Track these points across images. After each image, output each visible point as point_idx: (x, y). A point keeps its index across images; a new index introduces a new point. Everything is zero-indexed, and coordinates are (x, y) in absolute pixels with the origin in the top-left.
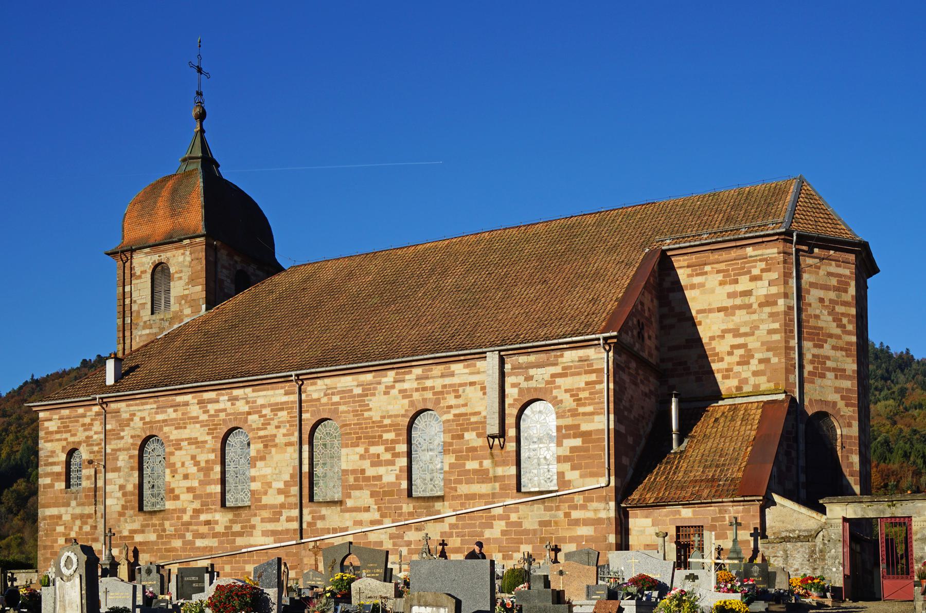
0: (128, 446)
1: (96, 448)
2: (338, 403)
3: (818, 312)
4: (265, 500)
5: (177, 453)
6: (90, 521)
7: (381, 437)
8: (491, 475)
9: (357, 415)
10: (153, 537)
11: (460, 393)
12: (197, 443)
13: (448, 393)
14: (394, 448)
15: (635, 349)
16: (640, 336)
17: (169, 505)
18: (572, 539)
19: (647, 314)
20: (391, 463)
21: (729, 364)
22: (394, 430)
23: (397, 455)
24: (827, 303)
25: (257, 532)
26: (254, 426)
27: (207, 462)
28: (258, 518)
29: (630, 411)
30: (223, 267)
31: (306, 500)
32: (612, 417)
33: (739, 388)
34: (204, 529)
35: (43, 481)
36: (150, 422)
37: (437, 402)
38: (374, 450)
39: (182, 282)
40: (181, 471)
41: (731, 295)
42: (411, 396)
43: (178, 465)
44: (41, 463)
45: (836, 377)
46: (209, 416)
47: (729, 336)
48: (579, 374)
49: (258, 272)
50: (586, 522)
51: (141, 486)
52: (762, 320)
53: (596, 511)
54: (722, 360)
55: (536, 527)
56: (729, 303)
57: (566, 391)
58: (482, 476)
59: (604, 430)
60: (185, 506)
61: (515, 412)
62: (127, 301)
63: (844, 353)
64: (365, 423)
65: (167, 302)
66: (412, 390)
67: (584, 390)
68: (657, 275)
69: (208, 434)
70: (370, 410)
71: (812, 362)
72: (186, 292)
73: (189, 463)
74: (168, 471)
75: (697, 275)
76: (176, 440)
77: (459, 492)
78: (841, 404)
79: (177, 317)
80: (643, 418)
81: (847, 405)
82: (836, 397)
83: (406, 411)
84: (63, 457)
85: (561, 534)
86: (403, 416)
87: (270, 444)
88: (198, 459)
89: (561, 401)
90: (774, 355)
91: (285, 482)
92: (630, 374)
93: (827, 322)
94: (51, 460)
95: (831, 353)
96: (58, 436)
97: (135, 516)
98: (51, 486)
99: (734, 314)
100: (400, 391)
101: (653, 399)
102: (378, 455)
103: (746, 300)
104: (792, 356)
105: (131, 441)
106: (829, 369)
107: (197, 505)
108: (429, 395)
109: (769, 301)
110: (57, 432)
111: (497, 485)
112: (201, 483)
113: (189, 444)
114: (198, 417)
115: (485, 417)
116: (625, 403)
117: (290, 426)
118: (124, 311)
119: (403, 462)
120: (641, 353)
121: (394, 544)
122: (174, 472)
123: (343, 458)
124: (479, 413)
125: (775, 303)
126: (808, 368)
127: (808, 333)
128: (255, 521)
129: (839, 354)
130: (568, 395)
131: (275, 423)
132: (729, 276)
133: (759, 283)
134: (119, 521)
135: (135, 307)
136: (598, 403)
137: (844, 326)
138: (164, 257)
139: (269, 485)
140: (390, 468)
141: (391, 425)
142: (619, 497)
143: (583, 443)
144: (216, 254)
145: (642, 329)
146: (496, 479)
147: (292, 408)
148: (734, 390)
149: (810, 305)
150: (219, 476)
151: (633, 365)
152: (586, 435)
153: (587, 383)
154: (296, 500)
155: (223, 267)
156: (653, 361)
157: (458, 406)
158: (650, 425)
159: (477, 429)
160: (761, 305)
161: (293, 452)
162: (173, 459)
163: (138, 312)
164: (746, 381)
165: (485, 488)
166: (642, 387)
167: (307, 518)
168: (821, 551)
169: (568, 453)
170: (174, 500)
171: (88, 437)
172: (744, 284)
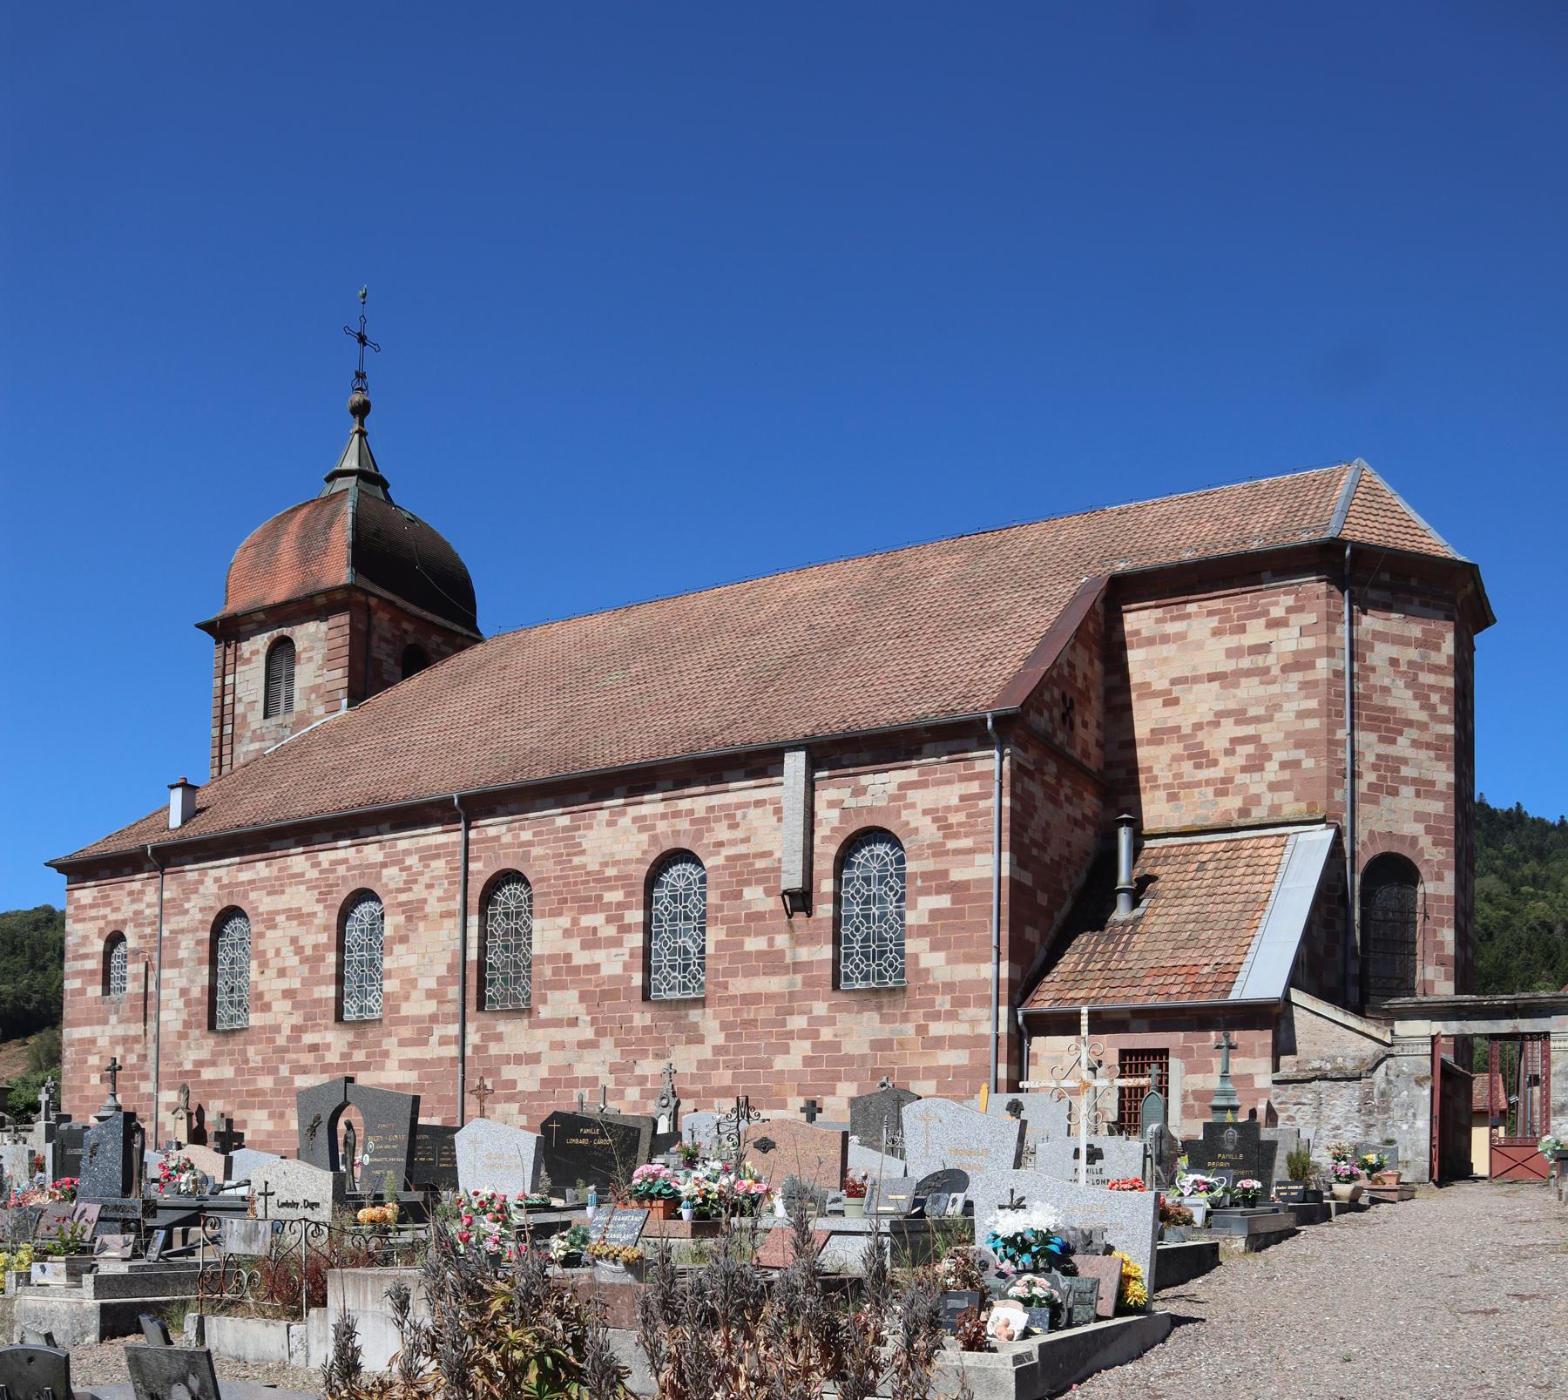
0: (196, 924)
1: (148, 930)
2: (530, 844)
3: (1387, 682)
4: (407, 1009)
5: (270, 934)
6: (138, 1048)
7: (600, 897)
8: (788, 960)
9: (560, 863)
10: (228, 1072)
11: (738, 819)
12: (302, 915)
13: (718, 819)
14: (621, 917)
15: (1057, 742)
16: (1067, 720)
17: (255, 1019)
18: (930, 1073)
19: (1080, 684)
20: (616, 942)
21: (1226, 770)
22: (623, 886)
23: (625, 929)
24: (1403, 668)
25: (391, 1063)
26: (392, 886)
27: (315, 947)
28: (394, 1040)
29: (1042, 847)
30: (382, 639)
31: (471, 1008)
32: (1006, 856)
33: (1244, 812)
34: (307, 1059)
35: (69, 985)
36: (230, 885)
37: (698, 836)
38: (587, 920)
39: (313, 666)
40: (275, 963)
41: (1231, 653)
42: (653, 827)
43: (271, 954)
44: (68, 955)
45: (1418, 794)
46: (321, 872)
47: (1227, 723)
48: (949, 782)
49: (444, 648)
50: (955, 1042)
51: (212, 990)
52: (1288, 696)
53: (973, 1022)
54: (1215, 763)
55: (866, 1050)
56: (1229, 666)
57: (925, 812)
58: (772, 962)
59: (990, 879)
60: (279, 1020)
61: (833, 849)
62: (228, 699)
63: (1432, 754)
64: (576, 876)
65: (290, 698)
66: (655, 816)
67: (957, 809)
68: (1101, 619)
69: (318, 901)
70: (583, 852)
71: (1375, 767)
72: (319, 680)
73: (287, 950)
74: (254, 964)
75: (1173, 619)
76: (268, 913)
77: (732, 991)
78: (1425, 841)
79: (303, 721)
80: (1069, 860)
81: (1435, 844)
82: (1418, 829)
83: (644, 852)
84: (99, 946)
85: (910, 1063)
86: (639, 861)
87: (416, 914)
88: (301, 943)
89: (916, 829)
90: (1308, 755)
91: (439, 978)
92: (1044, 784)
93: (1402, 700)
94: (82, 951)
95: (1410, 753)
96: (93, 913)
97: (204, 1037)
98: (82, 992)
99: (1236, 685)
100: (635, 820)
101: (1090, 831)
102: (595, 929)
103: (1260, 661)
104: (1340, 755)
105: (199, 916)
106: (1405, 781)
107: (297, 1019)
108: (684, 824)
109: (1300, 663)
110: (92, 906)
111: (799, 978)
112: (304, 981)
113: (288, 918)
114: (302, 875)
115: (780, 861)
116: (1033, 833)
117: (450, 884)
118: (222, 715)
119: (636, 940)
120: (1068, 750)
121: (618, 1082)
122: (264, 965)
123: (535, 937)
124: (767, 854)
125: (1311, 666)
126: (1370, 777)
127: (1369, 718)
128: (390, 1043)
129: (1424, 755)
130: (928, 819)
131: (425, 879)
132: (1230, 620)
133: (1283, 632)
134: (179, 1046)
135: (239, 709)
136: (982, 833)
137: (1433, 708)
138: (286, 631)
139: (413, 983)
140: (614, 951)
141: (617, 878)
142: (1018, 997)
143: (953, 903)
144: (370, 618)
145: (1071, 708)
146: (797, 967)
147: (453, 854)
148: (1235, 815)
149: (1373, 669)
150: (333, 971)
151: (1052, 768)
152: (958, 889)
153: (963, 798)
154: (454, 1008)
155: (382, 639)
156: (1093, 764)
157: (733, 843)
158: (1083, 875)
159: (767, 880)
160: (1285, 669)
161: (452, 927)
162: (263, 944)
163: (244, 717)
164: (1256, 800)
165: (775, 984)
166: (1068, 809)
167: (473, 1038)
168: (1383, 1094)
169: (925, 921)
170: (262, 1010)
171: (137, 913)
172: (1257, 632)
